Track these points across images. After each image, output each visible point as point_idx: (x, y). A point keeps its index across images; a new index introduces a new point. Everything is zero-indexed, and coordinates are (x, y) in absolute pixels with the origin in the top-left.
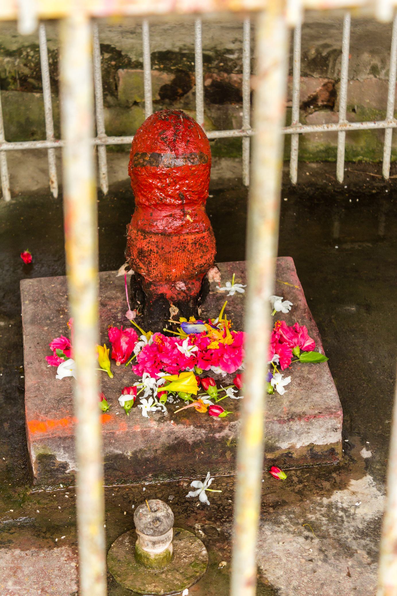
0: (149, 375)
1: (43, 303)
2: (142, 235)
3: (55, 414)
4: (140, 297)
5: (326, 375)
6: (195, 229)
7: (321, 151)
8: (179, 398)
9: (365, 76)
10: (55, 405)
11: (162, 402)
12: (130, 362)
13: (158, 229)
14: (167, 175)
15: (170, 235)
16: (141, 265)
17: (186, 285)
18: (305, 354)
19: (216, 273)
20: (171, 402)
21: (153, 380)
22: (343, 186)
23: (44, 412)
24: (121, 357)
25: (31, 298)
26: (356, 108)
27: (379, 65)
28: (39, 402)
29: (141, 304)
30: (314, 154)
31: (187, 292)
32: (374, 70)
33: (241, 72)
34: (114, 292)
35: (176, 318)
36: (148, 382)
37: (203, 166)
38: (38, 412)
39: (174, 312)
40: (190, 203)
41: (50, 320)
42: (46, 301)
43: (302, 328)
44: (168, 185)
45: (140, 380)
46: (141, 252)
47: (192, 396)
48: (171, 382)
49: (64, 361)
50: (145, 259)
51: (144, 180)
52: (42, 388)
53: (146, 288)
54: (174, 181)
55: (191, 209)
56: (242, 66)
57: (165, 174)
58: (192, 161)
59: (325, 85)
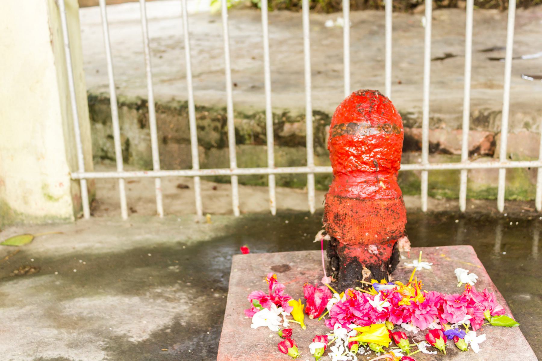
0: (340, 326)
1: (250, 271)
2: (338, 200)
3: (245, 359)
4: (335, 264)
5: (519, 338)
6: (388, 195)
7: (483, 191)
8: (370, 350)
9: (519, 129)
10: (247, 350)
11: (354, 352)
12: (323, 316)
13: (353, 195)
14: (363, 143)
15: (364, 199)
16: (337, 229)
17: (378, 249)
18: (496, 318)
19: (406, 242)
20: (362, 353)
21: (345, 331)
22: (503, 214)
23: (235, 356)
24: (314, 311)
25: (239, 267)
26: (512, 156)
27: (531, 121)
28: (232, 347)
29: (336, 271)
30: (477, 193)
31: (379, 256)
32: (527, 125)
33: (420, 127)
34: (313, 265)
35: (368, 279)
36: (339, 333)
37: (396, 135)
38: (229, 355)
39: (366, 274)
40: (384, 171)
41: (254, 283)
42: (252, 270)
43: (491, 294)
44: (363, 153)
45: (331, 332)
46: (337, 216)
47: (384, 347)
48: (362, 333)
49: (259, 310)
50: (341, 222)
51: (342, 149)
52: (237, 336)
53: (341, 251)
54: (369, 149)
55: (384, 176)
56: (421, 123)
57: (361, 142)
58: (386, 130)
59: (487, 137)
